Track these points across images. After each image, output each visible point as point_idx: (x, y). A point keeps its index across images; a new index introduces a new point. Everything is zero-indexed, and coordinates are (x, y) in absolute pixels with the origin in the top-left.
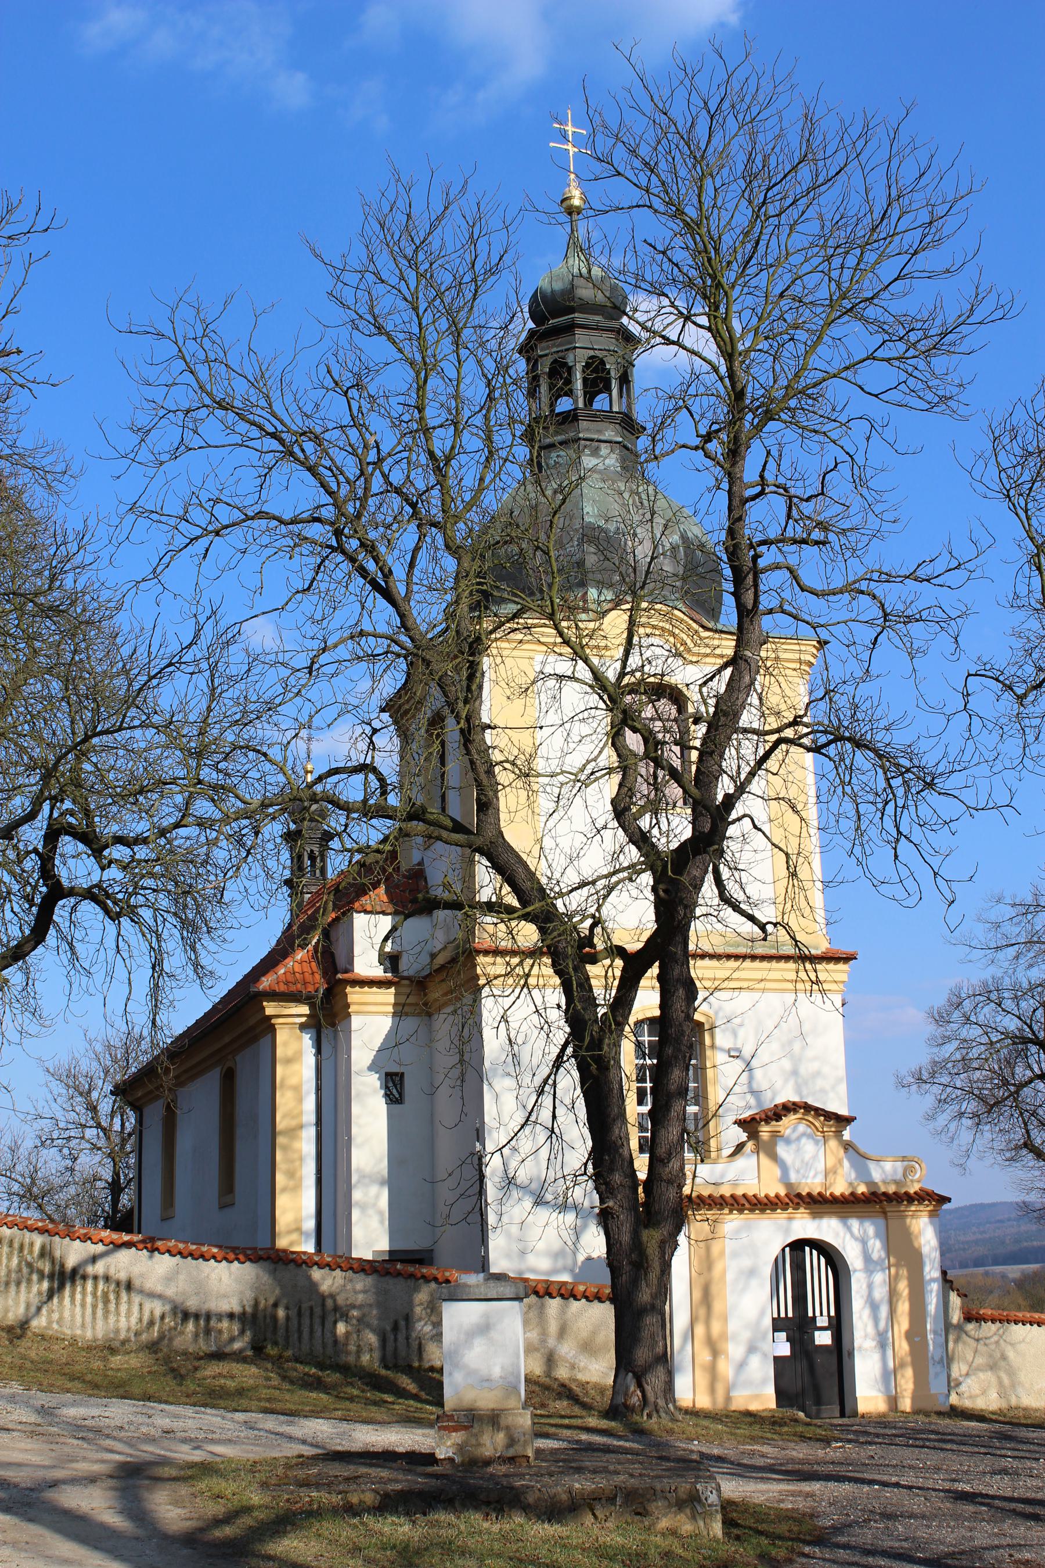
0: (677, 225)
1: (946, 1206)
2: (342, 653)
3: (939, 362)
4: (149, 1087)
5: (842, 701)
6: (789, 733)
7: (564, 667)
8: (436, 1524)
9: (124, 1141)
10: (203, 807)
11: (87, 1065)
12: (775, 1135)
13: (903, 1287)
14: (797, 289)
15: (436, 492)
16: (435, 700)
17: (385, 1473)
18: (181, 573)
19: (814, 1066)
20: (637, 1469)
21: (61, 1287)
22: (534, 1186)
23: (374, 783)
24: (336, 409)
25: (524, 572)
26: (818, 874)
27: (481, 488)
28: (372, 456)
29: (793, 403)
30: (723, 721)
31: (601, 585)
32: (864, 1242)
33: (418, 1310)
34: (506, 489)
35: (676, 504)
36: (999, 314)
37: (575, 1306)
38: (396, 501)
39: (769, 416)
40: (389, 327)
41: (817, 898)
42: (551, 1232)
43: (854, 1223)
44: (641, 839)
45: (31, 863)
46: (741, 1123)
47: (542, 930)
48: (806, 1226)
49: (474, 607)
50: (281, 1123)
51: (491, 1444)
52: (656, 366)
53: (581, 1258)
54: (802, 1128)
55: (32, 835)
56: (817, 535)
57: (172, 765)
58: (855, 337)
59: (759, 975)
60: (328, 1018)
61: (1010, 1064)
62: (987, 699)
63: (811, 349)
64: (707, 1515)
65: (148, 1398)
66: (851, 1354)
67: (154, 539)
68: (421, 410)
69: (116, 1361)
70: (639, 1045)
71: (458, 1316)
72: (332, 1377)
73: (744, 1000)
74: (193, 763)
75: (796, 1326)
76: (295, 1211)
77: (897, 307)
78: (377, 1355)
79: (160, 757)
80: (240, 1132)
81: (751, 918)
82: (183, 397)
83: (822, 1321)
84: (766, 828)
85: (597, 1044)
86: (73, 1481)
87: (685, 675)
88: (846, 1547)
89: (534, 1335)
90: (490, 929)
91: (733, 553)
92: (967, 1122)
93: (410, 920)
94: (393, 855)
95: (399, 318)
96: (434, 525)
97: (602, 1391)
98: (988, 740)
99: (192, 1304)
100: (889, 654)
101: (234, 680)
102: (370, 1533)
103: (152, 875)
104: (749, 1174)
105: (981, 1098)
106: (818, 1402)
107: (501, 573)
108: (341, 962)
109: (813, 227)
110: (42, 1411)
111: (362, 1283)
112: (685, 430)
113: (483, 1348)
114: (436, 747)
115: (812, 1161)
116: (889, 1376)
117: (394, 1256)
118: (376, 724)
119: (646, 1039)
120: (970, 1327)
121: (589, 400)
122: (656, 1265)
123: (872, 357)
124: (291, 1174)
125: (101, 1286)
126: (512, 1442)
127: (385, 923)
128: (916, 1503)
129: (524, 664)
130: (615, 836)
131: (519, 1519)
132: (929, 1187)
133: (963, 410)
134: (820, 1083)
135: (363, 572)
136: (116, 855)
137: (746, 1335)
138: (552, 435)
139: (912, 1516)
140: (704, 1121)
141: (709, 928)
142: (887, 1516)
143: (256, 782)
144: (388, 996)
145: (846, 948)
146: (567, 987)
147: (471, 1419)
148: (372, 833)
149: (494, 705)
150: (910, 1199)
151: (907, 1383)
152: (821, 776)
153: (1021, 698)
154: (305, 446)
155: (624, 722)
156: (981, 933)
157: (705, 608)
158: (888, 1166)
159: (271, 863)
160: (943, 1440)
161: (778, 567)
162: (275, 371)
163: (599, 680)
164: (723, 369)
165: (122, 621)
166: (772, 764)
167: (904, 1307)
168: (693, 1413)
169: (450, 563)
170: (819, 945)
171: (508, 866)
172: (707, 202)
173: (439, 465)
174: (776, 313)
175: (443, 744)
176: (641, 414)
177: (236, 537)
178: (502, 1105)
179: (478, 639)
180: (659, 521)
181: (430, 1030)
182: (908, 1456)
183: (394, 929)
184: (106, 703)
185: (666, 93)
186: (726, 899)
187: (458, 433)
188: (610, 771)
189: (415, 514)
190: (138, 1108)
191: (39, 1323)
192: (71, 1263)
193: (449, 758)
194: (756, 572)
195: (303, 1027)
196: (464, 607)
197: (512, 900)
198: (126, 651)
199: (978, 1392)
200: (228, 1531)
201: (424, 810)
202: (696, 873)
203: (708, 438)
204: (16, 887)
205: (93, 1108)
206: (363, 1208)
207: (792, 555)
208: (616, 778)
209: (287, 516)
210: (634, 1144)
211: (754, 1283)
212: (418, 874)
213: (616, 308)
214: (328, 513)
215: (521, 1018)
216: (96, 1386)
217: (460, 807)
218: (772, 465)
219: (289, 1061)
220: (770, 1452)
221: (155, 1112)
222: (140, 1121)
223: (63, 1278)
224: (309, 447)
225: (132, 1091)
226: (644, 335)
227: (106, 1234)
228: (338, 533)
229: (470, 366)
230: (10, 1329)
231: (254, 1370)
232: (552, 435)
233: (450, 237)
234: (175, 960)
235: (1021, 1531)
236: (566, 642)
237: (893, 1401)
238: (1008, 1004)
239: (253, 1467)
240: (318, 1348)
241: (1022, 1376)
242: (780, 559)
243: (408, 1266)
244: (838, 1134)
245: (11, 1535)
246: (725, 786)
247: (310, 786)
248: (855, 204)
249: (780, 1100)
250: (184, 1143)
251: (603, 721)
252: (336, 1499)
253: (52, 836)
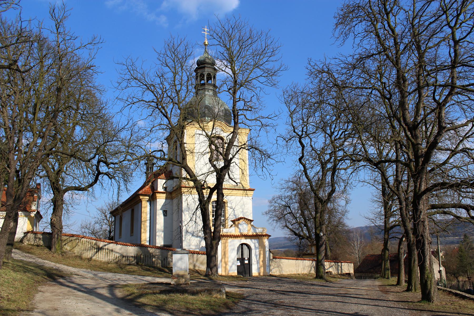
0: (225, 49)
1: (270, 237)
2: (157, 128)
3: (274, 77)
4: (117, 212)
5: (253, 141)
6: (243, 146)
7: (201, 132)
8: (171, 296)
9: (112, 223)
10: (129, 157)
11: (105, 208)
12: (239, 223)
13: (262, 252)
14: (248, 62)
15: (176, 97)
16: (175, 138)
17: (161, 287)
18: (126, 111)
19: (246, 210)
20: (210, 286)
21: (99, 251)
22: (192, 232)
23: (163, 154)
24: (158, 80)
25: (193, 114)
26: (248, 174)
27: (185, 97)
28: (164, 90)
29: (246, 84)
30: (231, 144)
31: (208, 117)
32: (255, 244)
33: (169, 256)
34: (190, 98)
35: (223, 102)
37: (199, 256)
38: (169, 99)
39: (241, 86)
40: (169, 65)
41: (248, 178)
42: (195, 241)
43: (253, 240)
44: (214, 166)
45: (94, 167)
46: (232, 221)
47: (194, 183)
48: (244, 241)
49: (183, 120)
50: (143, 219)
51: (182, 281)
52: (220, 75)
53: (201, 246)
54: (244, 222)
55: (95, 162)
56: (250, 109)
57: (123, 149)
58: (258, 72)
59: (229, 193)
60: (152, 200)
61: (283, 211)
62: (281, 141)
63: (250, 74)
64: (222, 294)
65: (115, 272)
66: (252, 265)
67: (121, 104)
68: (174, 81)
69: (109, 265)
70: (213, 206)
71: (176, 257)
72: (152, 269)
73: (233, 197)
74: (127, 148)
75: (241, 260)
76: (145, 237)
77: (266, 67)
78: (161, 265)
79: (120, 148)
80: (135, 221)
81: (235, 182)
82: (128, 77)
83: (246, 259)
84: (238, 165)
85: (204, 205)
86: (100, 288)
87: (224, 135)
88: (249, 300)
89: (191, 261)
90: (184, 183)
91: (234, 111)
92: (275, 222)
93: (169, 181)
94: (166, 167)
95: (171, 64)
96: (176, 104)
97: (204, 272)
98: (281, 149)
99: (125, 254)
100: (263, 132)
101: (136, 132)
102: (158, 298)
103: (118, 170)
104: (233, 231)
105: (278, 217)
106: (245, 274)
107: (189, 114)
108: (155, 188)
109: (251, 51)
110: (94, 275)
111: (158, 251)
112: (225, 88)
113: (181, 263)
114: (175, 147)
115: (245, 228)
116: (259, 269)
117: (164, 246)
118: (163, 142)
119: (214, 205)
120: (274, 260)
121: (207, 81)
122: (215, 248)
123: (261, 76)
124: (145, 229)
125: (107, 250)
126: (186, 281)
127: (164, 181)
128: (262, 292)
129: (193, 131)
131: (187, 295)
132: (267, 233)
133: (278, 87)
134: (247, 214)
135: (162, 112)
136: (111, 166)
137: (232, 261)
138: (200, 88)
139: (261, 294)
140: (225, 221)
141: (227, 183)
142: (257, 294)
143: (139, 153)
144: (164, 195)
145: (253, 188)
146: (199, 194)
147: (179, 276)
148: (162, 163)
149: (186, 139)
150: (264, 236)
151: (262, 270)
152: (249, 155)
153: (287, 141)
155: (211, 143)
156: (278, 186)
157: (228, 122)
158: (260, 229)
159: (142, 169)
160: (268, 280)
161: (242, 115)
163: (207, 135)
164: (233, 76)
165: (114, 120)
166: (240, 152)
167: (262, 256)
168: (221, 276)
169: (179, 111)
170: (248, 187)
171: (189, 171)
172: (231, 45)
173: (178, 92)
174: (243, 66)
175: (176, 146)
176: (217, 84)
177: (137, 105)
178: (186, 217)
179: (184, 126)
180: (220, 105)
181: (172, 202)
182: (261, 283)
183: (165, 182)
184: (111, 136)
185: (224, 24)
186: (230, 178)
187: (181, 86)
188: (208, 153)
189: (172, 101)
190: (115, 216)
191: (94, 258)
192: (101, 246)
193: (178, 149)
194: (238, 115)
195: (147, 201)
196: (181, 120)
197: (189, 177)
198: (114, 126)
199: (275, 272)
200: (130, 297)
201: (172, 159)
202: (224, 173)
203: (229, 89)
204: (91, 172)
205: (106, 216)
206: (159, 236)
207: (245, 112)
208: (210, 154)
209: (147, 101)
210: (211, 225)
211: (234, 251)
212: (171, 172)
213: (213, 64)
214: (155, 101)
215: (190, 200)
216: (105, 270)
217: (179, 159)
218: (241, 95)
219: (145, 207)
220: (236, 283)
221: (118, 217)
222: (115, 219)
223: (99, 249)
224: (152, 88)
225: (113, 213)
226: (218, 69)
227: (108, 241)
228: (157, 105)
229: (184, 73)
230: (88, 259)
231: (136, 267)
232: (200, 88)
233: (181, 48)
234: (123, 187)
235: (281, 296)
236: (201, 127)
237: (259, 273)
238: (283, 199)
239: (135, 286)
240: (149, 263)
241: (283, 269)
242: (242, 113)
243: (168, 248)
244: (250, 223)
245: (87, 298)
246: (230, 156)
247: (150, 154)
248: (259, 47)
249: (240, 217)
250: (124, 224)
251: (208, 143)
252: (151, 291)
253: (99, 162)
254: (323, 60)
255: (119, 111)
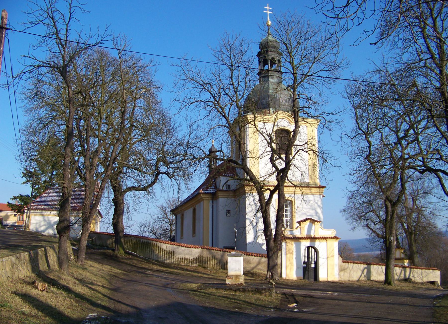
4: (178, 210)
11: (165, 205)
23: (222, 155)
36: (347, 64)
62: (345, 139)
80: (197, 221)
130: (270, 165)
154: (208, 86)
162: (201, 72)
190: (176, 215)
221: (179, 216)
225: (173, 211)
233: (237, 44)
234: (183, 187)
250: (185, 223)
254: (372, 68)
255: (176, 112)
